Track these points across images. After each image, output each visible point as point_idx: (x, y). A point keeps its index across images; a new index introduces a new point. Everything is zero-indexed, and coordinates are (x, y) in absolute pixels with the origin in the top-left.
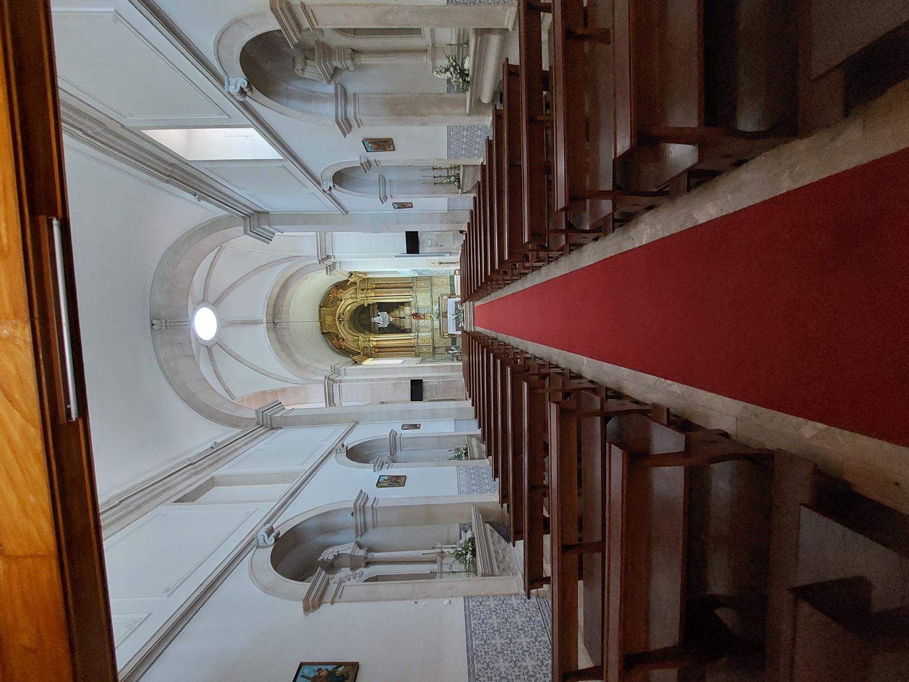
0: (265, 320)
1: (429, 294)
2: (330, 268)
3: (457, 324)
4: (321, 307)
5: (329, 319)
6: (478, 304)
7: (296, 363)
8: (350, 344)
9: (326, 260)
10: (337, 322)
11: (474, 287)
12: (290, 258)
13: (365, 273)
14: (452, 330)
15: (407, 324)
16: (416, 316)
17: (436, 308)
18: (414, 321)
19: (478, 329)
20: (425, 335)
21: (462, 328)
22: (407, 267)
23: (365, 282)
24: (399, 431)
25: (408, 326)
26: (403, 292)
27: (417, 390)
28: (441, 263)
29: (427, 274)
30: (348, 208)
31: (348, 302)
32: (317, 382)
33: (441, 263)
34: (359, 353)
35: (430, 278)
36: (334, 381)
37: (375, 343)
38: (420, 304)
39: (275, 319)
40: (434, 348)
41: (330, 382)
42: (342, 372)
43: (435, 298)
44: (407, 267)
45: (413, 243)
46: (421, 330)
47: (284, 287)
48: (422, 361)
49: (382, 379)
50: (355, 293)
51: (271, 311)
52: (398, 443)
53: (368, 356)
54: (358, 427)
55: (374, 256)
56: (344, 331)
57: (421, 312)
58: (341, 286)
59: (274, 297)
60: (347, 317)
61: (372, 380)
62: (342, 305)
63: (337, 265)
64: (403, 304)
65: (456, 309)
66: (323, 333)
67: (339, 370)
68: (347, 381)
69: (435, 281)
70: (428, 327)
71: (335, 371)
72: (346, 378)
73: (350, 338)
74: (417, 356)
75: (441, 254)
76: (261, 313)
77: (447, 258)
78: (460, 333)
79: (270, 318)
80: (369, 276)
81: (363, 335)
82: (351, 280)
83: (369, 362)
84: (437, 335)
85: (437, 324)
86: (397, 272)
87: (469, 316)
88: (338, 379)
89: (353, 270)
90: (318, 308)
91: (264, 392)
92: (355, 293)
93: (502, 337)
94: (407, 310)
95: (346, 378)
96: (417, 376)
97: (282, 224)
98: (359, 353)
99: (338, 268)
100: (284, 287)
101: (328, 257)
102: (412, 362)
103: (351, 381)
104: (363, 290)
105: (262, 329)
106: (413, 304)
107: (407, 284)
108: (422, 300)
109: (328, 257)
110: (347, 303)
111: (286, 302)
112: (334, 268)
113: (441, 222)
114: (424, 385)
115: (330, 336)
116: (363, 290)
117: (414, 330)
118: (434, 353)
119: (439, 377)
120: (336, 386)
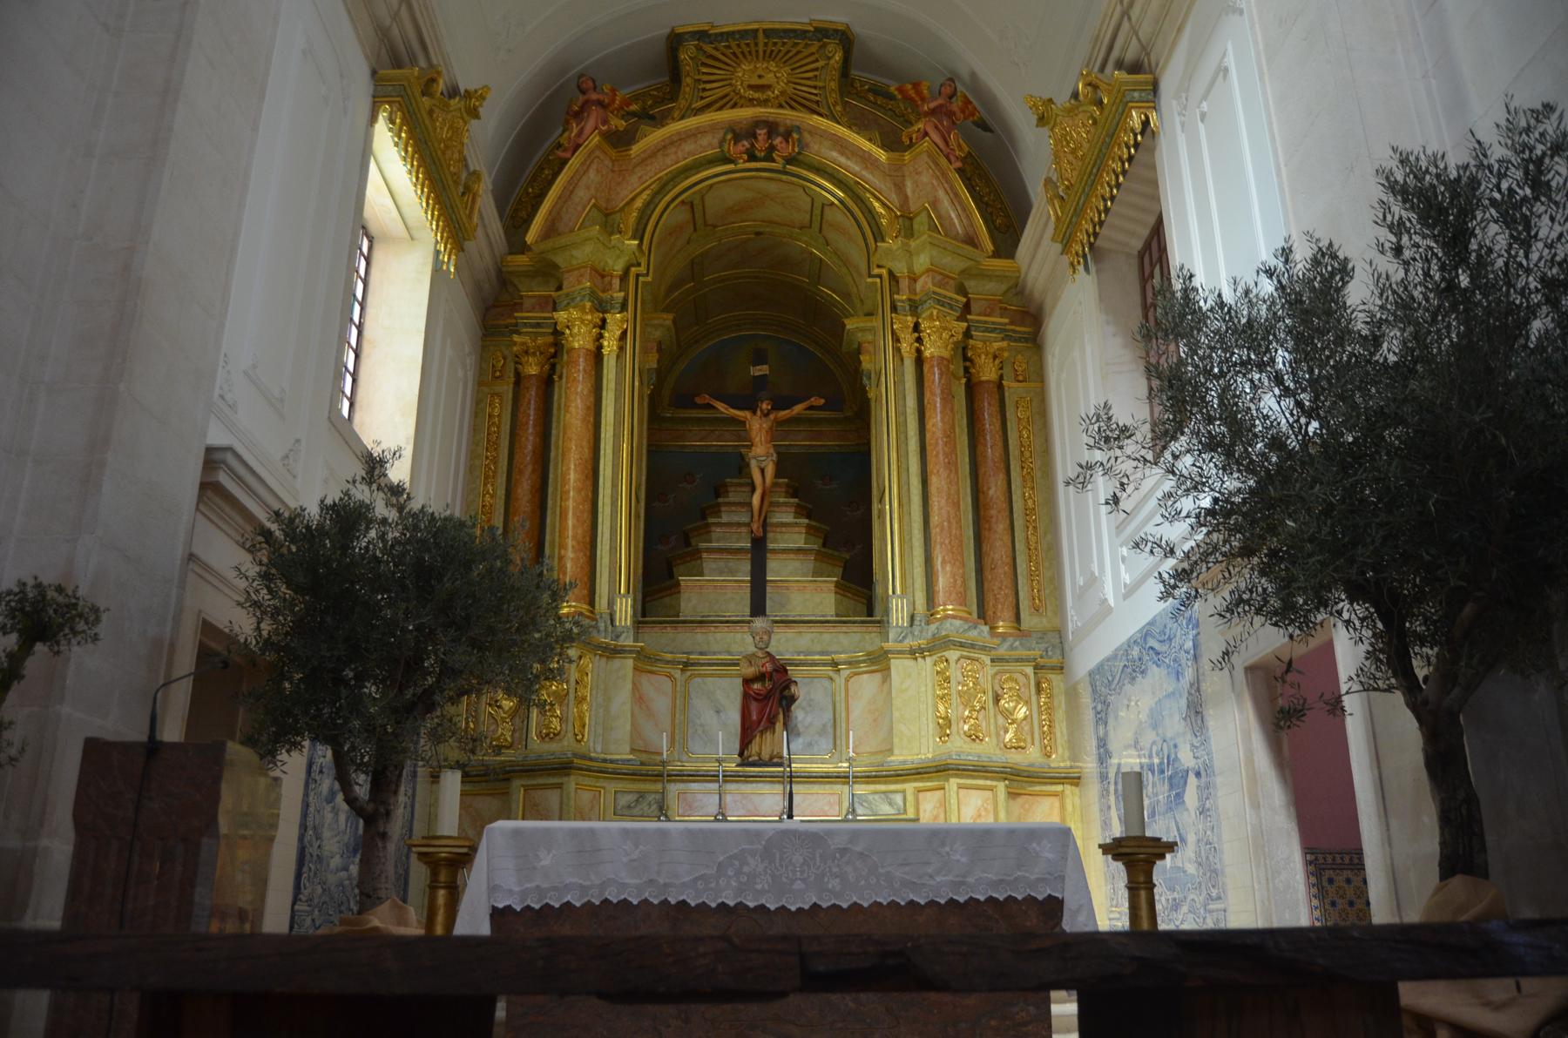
4: (845, 38)
8: (582, 178)
15: (715, 586)
34: (516, 243)
37: (579, 339)
46: (659, 692)
66: (675, 41)
70: (680, 733)
73: (635, 188)
90: (836, 17)
94: (804, 589)
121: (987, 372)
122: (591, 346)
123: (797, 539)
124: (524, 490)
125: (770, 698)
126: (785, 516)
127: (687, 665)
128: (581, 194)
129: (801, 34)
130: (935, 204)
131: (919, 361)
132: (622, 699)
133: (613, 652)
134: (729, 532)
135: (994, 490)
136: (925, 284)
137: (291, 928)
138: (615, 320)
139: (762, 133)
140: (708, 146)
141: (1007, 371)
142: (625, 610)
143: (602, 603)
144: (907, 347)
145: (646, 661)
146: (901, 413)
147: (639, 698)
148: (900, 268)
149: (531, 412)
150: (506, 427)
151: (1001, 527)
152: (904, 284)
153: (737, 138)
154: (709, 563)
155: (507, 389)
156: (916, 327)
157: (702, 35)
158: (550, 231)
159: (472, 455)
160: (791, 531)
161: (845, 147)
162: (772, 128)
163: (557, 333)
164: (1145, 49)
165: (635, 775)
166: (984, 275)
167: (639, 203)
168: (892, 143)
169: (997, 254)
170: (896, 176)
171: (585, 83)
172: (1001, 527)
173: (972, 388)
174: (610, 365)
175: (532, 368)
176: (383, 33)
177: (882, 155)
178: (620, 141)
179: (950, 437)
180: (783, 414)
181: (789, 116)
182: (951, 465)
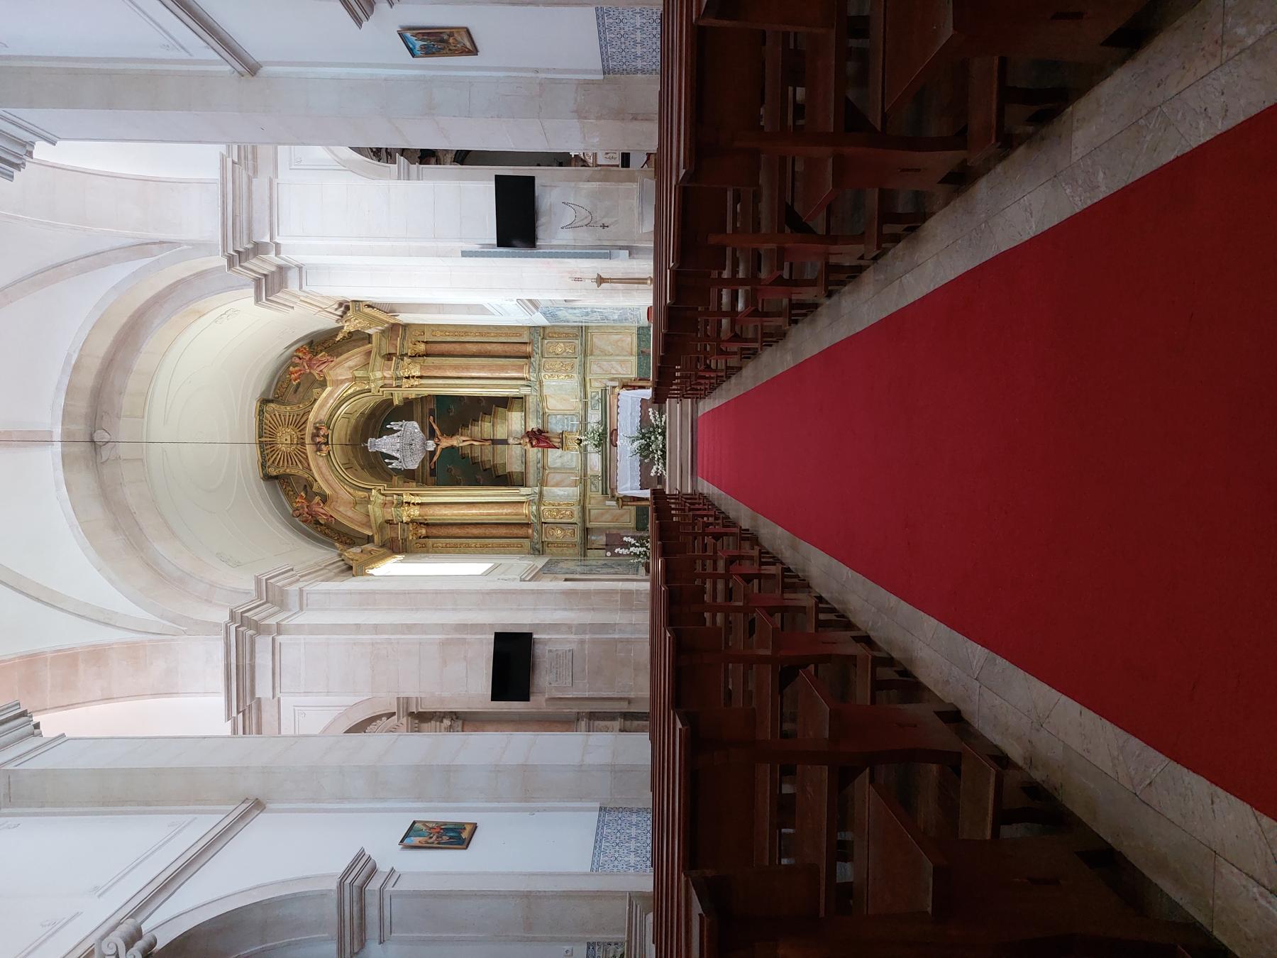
0: (57, 435)
1: (576, 377)
2: (270, 285)
3: (645, 468)
4: (265, 401)
5: (285, 438)
6: (706, 406)
7: (152, 565)
8: (344, 512)
9: (253, 260)
10: (309, 449)
11: (683, 349)
12: (142, 248)
13: (390, 309)
14: (629, 484)
15: (512, 458)
16: (539, 437)
17: (594, 417)
18: (534, 453)
19: (706, 487)
20: (563, 493)
21: (660, 479)
22: (508, 291)
23: (397, 337)
24: (386, 849)
25: (515, 467)
26: (503, 368)
27: (513, 661)
28: (601, 280)
29: (572, 318)
30: (257, 55)
31: (342, 391)
32: (208, 628)
33: (601, 280)
34: (369, 539)
35: (582, 332)
36: (259, 629)
37: (415, 512)
38: (553, 404)
39: (96, 430)
40: (586, 531)
41: (246, 636)
42: (293, 600)
43: (595, 388)
44: (508, 291)
45: (517, 223)
46: (554, 477)
47: (131, 334)
48: (547, 570)
49: (409, 628)
50: (365, 365)
51: (82, 406)
52: (372, 913)
53: (395, 547)
54: (261, 821)
55: (419, 259)
56: (325, 472)
57: (555, 426)
58: (322, 345)
59: (94, 364)
60: (340, 431)
61: (376, 628)
62: (326, 400)
63: (293, 276)
64: (505, 403)
65: (644, 419)
66: (267, 478)
67: (282, 592)
68: (299, 629)
69: (598, 341)
70: (570, 471)
71: (271, 595)
72: (300, 619)
73: (344, 493)
74: (538, 551)
75: (603, 252)
76: (47, 411)
77: (621, 265)
78: (647, 493)
79: (80, 429)
80: (404, 318)
81: (383, 486)
82: (349, 327)
83: (392, 568)
84: (595, 494)
85: (595, 460)
86: (481, 309)
87: (678, 443)
88: (272, 621)
89: (350, 294)
90: (254, 405)
91: (32, 660)
92: (365, 365)
93: (774, 535)
94: (514, 422)
95: (300, 619)
96: (515, 619)
97: (31, 105)
98: (369, 539)
99: (293, 285)
100: (131, 334)
101: (258, 249)
102: (513, 570)
103: (315, 629)
104: (389, 357)
105: (49, 460)
106: (531, 403)
107: (516, 347)
108: (559, 394)
109: (258, 249)
110: (341, 391)
111: (133, 384)
112: (282, 284)
113: (581, 114)
114: (539, 650)
115: (285, 483)
116: (389, 357)
117: (531, 478)
118: (586, 546)
119: (582, 628)
120: (263, 643)
121: (422, 347)
122: (417, 507)
123: (487, 426)
124: (476, 531)
125: (539, 437)
126: (476, 429)
127: (544, 468)
128: (350, 514)
129: (261, 422)
130: (350, 368)
131: (421, 377)
132: (559, 491)
133: (541, 494)
134: (485, 454)
135: (473, 348)
136: (388, 374)
137: (641, 281)
138: (406, 498)
139: (318, 440)
140: (322, 462)
141: (420, 339)
142: (524, 490)
143: (523, 499)
144: (412, 382)
145: (542, 482)
146: (444, 386)
147: (557, 485)
148: (380, 383)
149: (443, 531)
150: (448, 540)
151: (489, 347)
152: (387, 382)
153: (319, 450)
154: (499, 461)
155: (430, 541)
156: (408, 378)
157: (263, 466)
158: (368, 525)
159: (454, 552)
160: (485, 428)
161: (324, 403)
162: (314, 436)
163: (412, 521)
164: (341, 305)
165: (585, 486)
166: (380, 349)
167: (352, 491)
168: (323, 384)
169: (370, 342)
170: (338, 383)
171: (297, 514)
172: (489, 347)
173: (427, 355)
174: (425, 500)
175: (423, 531)
176: (343, 571)
177: (329, 389)
178: (325, 499)
179: (455, 368)
180: (438, 432)
181: (309, 429)
182: (467, 368)
